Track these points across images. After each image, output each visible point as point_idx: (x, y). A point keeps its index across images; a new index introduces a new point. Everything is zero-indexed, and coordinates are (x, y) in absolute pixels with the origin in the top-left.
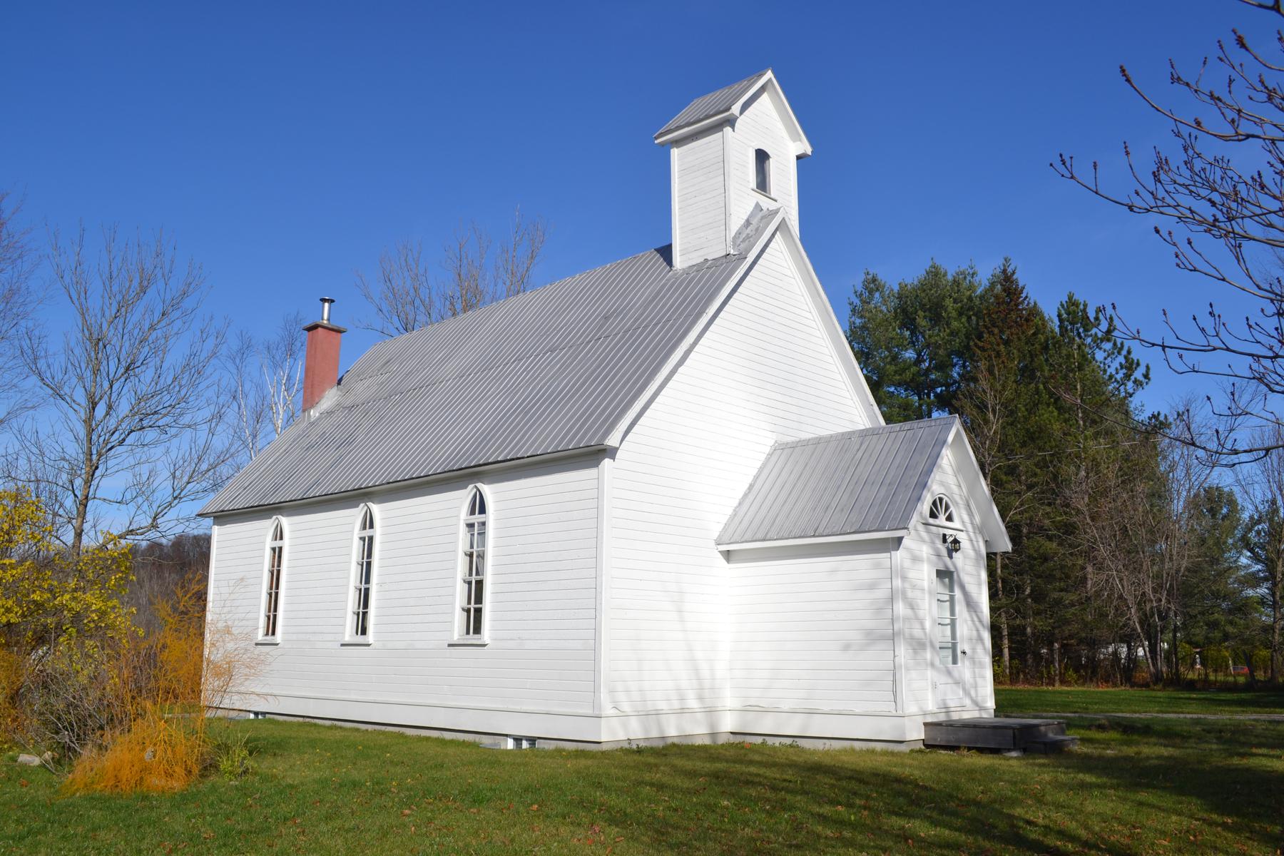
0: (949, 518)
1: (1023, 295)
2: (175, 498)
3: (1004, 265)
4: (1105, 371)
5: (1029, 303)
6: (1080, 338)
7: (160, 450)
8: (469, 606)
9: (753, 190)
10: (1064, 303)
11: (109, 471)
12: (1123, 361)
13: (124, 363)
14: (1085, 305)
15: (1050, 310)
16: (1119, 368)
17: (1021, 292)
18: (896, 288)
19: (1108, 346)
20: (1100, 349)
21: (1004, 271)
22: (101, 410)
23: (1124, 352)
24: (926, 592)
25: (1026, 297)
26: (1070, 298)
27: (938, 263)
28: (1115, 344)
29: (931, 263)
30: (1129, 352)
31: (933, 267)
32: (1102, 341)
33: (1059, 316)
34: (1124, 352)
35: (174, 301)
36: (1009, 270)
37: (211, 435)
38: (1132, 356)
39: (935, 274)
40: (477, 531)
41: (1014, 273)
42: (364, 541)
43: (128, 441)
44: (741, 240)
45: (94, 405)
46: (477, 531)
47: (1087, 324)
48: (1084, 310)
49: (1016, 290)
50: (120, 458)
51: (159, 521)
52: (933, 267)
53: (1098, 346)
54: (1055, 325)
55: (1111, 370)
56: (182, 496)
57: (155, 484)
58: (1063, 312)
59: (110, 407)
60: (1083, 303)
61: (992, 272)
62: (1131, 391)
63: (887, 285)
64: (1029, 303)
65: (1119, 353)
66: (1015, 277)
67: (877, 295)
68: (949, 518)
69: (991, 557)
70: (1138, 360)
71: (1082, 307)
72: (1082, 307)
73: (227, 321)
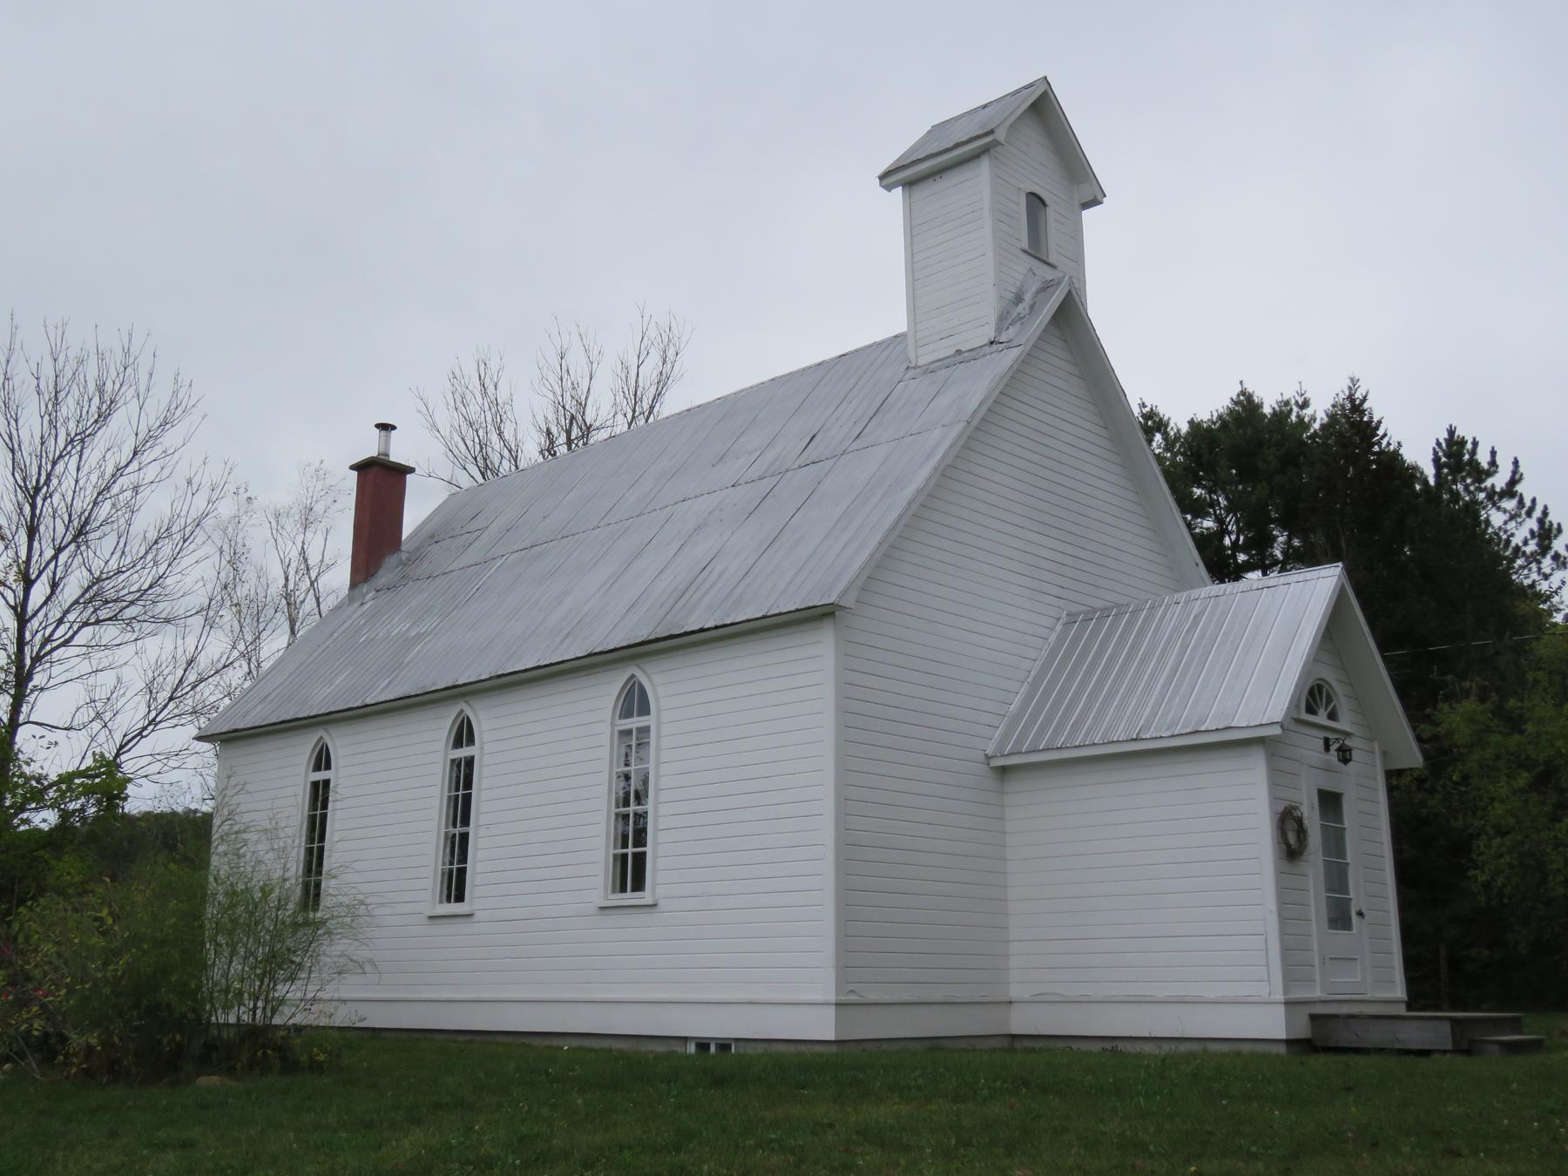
0: (1332, 716)
1: (1380, 432)
2: (150, 724)
3: (1350, 388)
4: (1508, 542)
5: (1389, 444)
6: (1469, 492)
7: (126, 652)
8: (625, 851)
9: (1025, 251)
10: (1442, 441)
11: (52, 682)
12: (1535, 527)
13: (76, 523)
14: (1475, 444)
15: (1419, 453)
16: (1529, 537)
17: (1377, 428)
18: (1185, 428)
19: (1509, 505)
20: (1499, 509)
21: (1351, 398)
22: (39, 592)
23: (1537, 513)
24: (1552, 553)
25: (1385, 435)
26: (1451, 432)
27: (1250, 390)
28: (1521, 503)
29: (1239, 389)
30: (1545, 513)
31: (1243, 393)
32: (1501, 498)
33: (1436, 460)
34: (1537, 513)
35: (151, 433)
36: (1358, 395)
37: (208, 628)
38: (1549, 518)
39: (1246, 407)
40: (633, 743)
41: (1364, 399)
42: (459, 765)
43: (78, 640)
44: (1010, 321)
45: (28, 583)
46: (633, 743)
47: (1480, 474)
48: (1473, 452)
49: (1371, 421)
50: (67, 661)
51: (123, 758)
52: (1243, 393)
53: (1494, 504)
54: (1430, 472)
55: (1517, 540)
56: (158, 719)
57: (120, 704)
58: (1440, 454)
59: (54, 585)
60: (1470, 441)
61: (1332, 402)
62: (1547, 571)
63: (1172, 424)
64: (1389, 444)
65: (1529, 514)
66: (1366, 406)
67: (1158, 437)
68: (1332, 716)
69: (1393, 776)
70: (1559, 525)
71: (1469, 446)
72: (1469, 446)
73: (228, 466)
